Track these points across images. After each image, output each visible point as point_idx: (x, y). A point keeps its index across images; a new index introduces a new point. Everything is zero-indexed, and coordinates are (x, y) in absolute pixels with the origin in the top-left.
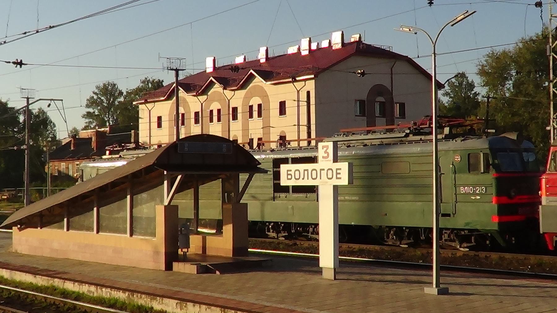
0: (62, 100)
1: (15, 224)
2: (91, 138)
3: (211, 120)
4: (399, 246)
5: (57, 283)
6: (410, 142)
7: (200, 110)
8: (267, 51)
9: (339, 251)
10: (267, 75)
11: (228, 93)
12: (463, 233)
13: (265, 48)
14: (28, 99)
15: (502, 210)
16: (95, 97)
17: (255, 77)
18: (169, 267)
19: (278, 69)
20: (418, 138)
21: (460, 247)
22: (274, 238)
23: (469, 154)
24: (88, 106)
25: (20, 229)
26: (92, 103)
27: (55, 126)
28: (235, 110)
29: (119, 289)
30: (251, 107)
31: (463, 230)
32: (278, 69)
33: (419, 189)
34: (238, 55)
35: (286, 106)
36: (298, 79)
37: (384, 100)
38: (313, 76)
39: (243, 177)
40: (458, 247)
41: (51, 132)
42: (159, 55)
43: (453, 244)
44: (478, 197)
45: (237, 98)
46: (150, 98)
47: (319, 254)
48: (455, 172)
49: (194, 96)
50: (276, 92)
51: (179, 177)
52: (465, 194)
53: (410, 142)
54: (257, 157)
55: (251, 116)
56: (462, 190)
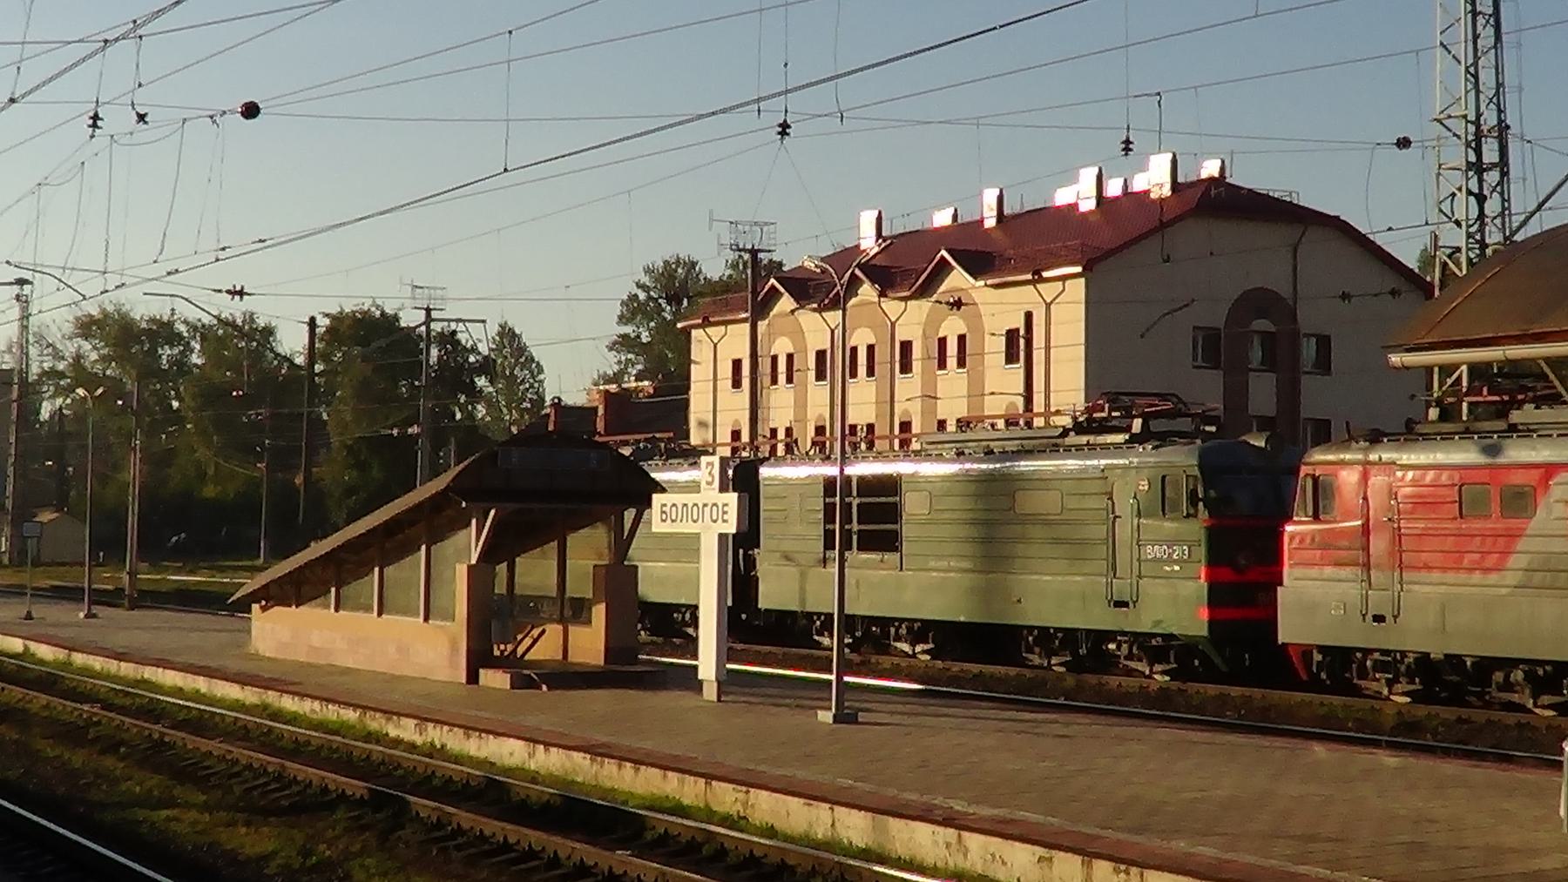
0: (484, 321)
1: (254, 597)
2: (595, 409)
3: (774, 381)
4: (1388, 698)
5: (272, 697)
6: (1068, 449)
7: (827, 346)
8: (1000, 199)
9: (726, 654)
10: (980, 262)
11: (892, 307)
12: (1154, 642)
13: (997, 191)
14: (428, 310)
15: (1217, 597)
16: (642, 296)
17: (953, 268)
18: (473, 678)
19: (989, 252)
20: (1084, 439)
21: (1535, 705)
22: (1040, 667)
23: (1164, 477)
24: (623, 320)
25: (264, 609)
26: (633, 310)
27: (541, 371)
28: (906, 347)
29: (348, 705)
30: (942, 342)
31: (1154, 635)
32: (989, 252)
33: (1073, 548)
34: (940, 207)
35: (693, 378)
36: (1046, 274)
37: (1273, 329)
38: (1079, 269)
39: (630, 515)
40: (1385, 692)
41: (532, 386)
42: (711, 212)
43: (1515, 698)
44: (1177, 568)
45: (911, 318)
46: (714, 314)
47: (696, 658)
48: (1139, 515)
49: (814, 310)
50: (999, 306)
51: (492, 512)
52: (1155, 560)
53: (1068, 449)
54: (653, 475)
55: (942, 364)
56: (1152, 551)
